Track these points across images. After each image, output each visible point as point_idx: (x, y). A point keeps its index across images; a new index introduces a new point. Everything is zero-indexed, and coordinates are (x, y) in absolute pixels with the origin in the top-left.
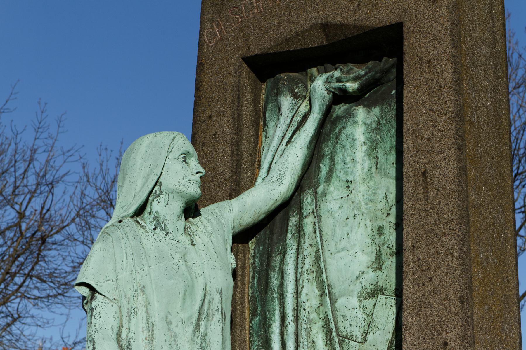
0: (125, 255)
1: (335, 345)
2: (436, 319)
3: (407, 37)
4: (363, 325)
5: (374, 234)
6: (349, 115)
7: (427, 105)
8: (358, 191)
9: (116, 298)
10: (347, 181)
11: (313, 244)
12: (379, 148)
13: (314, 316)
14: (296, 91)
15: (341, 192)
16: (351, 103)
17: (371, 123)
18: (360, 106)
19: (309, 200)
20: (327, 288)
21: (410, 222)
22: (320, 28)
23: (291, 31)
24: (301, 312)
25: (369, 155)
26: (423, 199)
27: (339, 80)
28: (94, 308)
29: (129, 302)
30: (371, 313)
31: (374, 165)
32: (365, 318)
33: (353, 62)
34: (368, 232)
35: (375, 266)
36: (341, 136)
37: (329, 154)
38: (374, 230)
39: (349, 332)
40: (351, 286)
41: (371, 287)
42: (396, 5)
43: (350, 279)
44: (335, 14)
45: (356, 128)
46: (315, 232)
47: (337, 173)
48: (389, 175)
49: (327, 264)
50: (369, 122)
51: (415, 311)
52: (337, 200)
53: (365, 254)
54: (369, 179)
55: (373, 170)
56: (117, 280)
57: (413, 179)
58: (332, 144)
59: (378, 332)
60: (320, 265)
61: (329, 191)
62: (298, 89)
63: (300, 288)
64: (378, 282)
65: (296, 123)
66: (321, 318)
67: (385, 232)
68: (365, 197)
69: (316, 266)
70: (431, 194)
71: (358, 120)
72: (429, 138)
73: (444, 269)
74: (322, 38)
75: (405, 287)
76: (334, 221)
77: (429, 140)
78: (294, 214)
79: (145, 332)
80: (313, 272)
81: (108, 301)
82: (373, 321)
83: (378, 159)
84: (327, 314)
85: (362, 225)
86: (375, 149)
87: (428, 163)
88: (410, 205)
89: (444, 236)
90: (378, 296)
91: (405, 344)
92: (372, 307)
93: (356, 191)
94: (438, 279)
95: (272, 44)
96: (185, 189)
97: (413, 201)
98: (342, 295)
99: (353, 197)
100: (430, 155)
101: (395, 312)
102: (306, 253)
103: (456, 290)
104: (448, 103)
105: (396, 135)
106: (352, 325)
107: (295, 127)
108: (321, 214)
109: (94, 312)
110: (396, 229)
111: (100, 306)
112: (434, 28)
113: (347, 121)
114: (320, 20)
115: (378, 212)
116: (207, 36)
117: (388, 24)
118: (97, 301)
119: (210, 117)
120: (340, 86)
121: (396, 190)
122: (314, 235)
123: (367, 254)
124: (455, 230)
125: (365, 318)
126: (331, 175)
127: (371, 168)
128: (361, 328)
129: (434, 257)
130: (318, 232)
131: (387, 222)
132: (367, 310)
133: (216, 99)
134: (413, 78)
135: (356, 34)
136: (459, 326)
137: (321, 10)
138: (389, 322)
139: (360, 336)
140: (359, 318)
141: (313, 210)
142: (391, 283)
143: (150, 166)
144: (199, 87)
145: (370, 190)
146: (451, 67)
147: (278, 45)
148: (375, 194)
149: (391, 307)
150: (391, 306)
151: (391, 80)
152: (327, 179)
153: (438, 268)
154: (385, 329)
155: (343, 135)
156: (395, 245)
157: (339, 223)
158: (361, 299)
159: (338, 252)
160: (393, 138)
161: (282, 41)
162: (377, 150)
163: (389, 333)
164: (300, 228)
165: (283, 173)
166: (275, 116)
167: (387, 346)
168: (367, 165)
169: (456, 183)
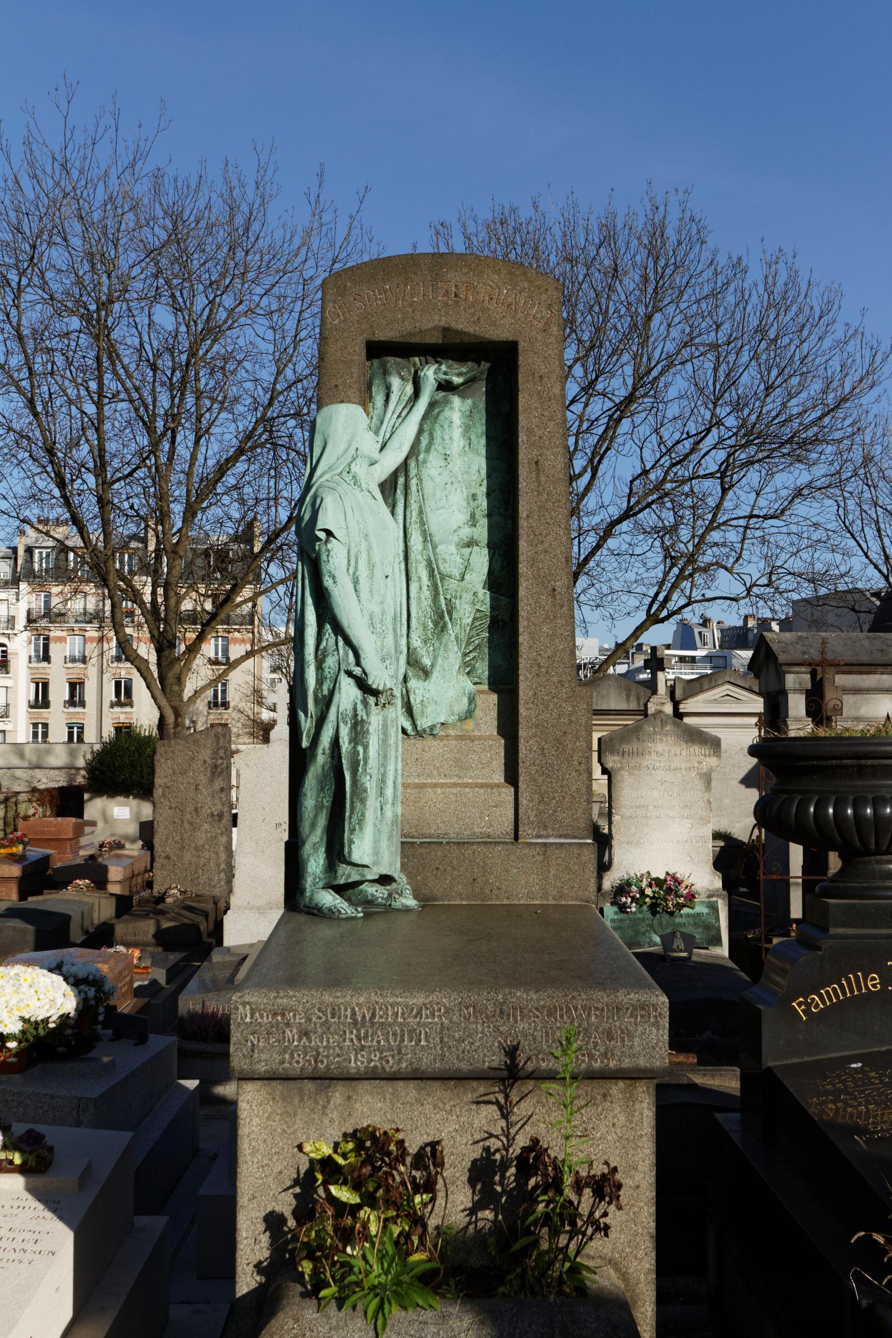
6: (447, 402)
7: (539, 410)
13: (419, 557)
25: (464, 436)
27: (445, 373)
31: (467, 444)
33: (453, 359)
35: (470, 523)
44: (457, 322)
55: (467, 448)
59: (474, 574)
70: (543, 479)
77: (540, 437)
85: (459, 490)
98: (441, 543)
102: (413, 507)
113: (445, 406)
119: (336, 386)
133: (342, 372)
136: (565, 578)
159: (438, 509)
164: (406, 487)
168: (462, 443)
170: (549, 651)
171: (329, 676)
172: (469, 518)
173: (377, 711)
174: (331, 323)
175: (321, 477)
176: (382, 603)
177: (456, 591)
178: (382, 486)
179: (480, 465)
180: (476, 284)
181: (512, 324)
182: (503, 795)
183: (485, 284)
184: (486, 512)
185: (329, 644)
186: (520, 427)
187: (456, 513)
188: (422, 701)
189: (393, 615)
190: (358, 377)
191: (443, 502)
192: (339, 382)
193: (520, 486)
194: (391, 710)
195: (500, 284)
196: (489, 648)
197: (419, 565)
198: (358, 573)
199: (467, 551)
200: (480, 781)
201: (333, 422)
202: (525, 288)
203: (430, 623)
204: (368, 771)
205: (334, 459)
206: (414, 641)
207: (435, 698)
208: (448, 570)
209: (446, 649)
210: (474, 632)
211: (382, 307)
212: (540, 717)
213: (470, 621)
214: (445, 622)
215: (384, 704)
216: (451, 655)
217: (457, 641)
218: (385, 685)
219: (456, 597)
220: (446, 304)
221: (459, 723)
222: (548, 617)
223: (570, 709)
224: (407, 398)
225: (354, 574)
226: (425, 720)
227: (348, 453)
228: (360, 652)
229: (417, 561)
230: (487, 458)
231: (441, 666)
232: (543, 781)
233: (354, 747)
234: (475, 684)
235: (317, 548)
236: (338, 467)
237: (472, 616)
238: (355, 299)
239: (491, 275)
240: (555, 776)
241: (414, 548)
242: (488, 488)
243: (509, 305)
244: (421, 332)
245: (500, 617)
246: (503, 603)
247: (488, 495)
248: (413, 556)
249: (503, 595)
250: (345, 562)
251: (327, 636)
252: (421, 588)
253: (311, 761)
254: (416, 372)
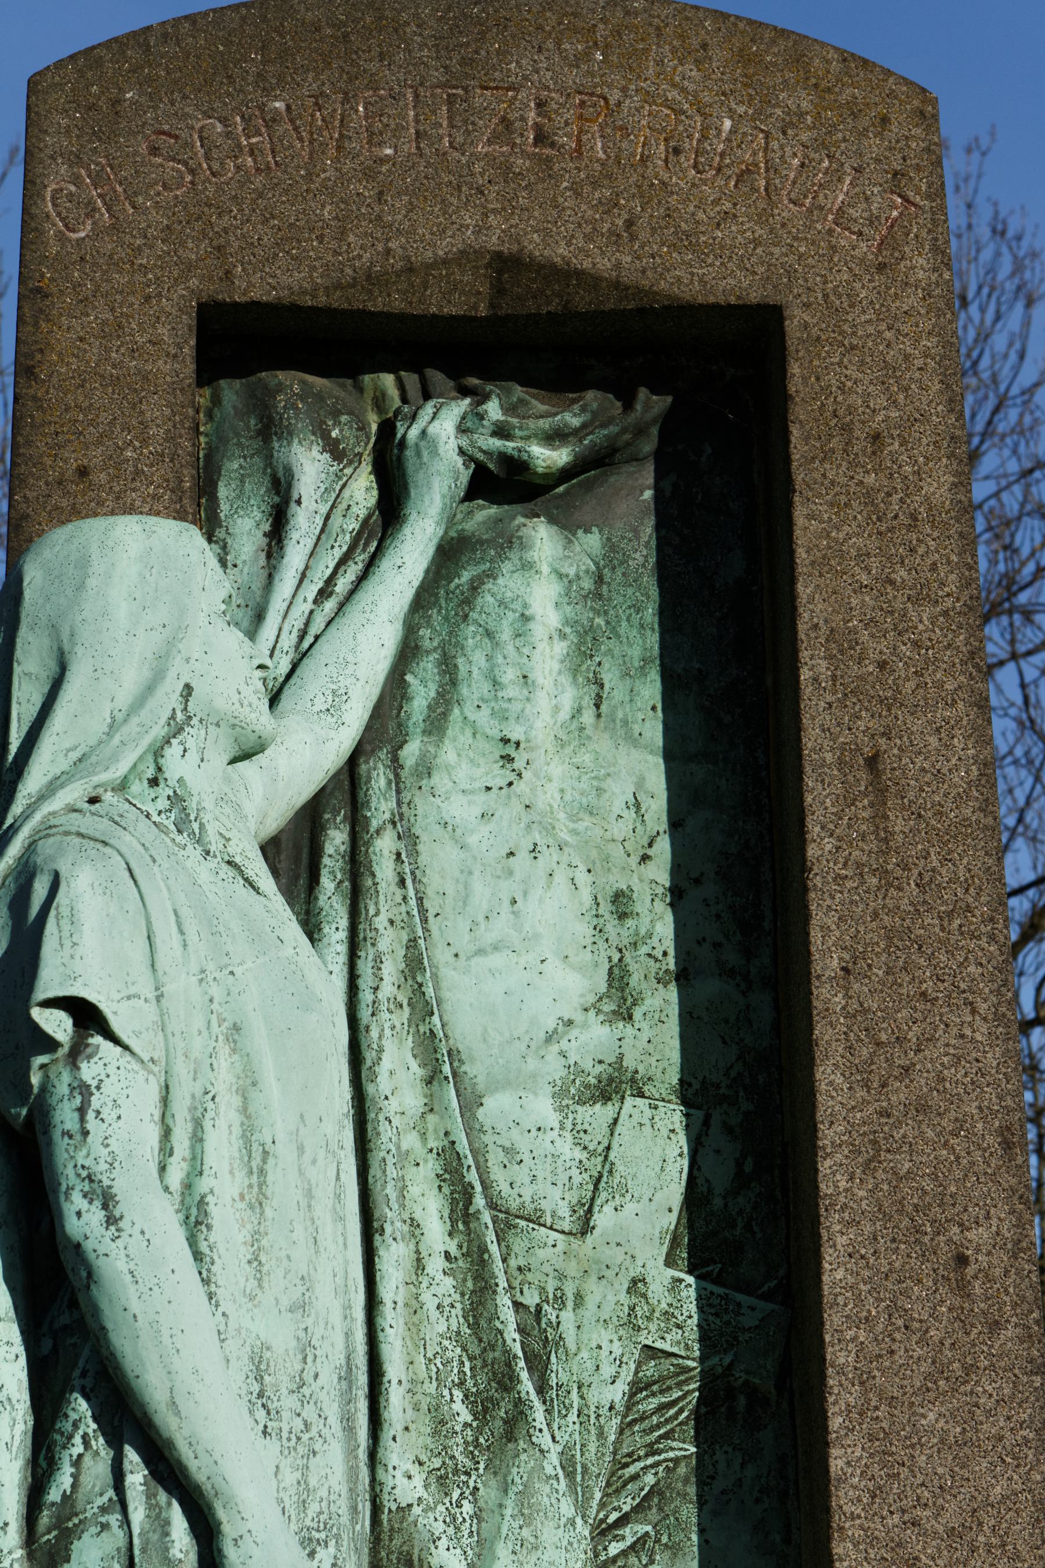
0: (173, 918)
1: (484, 1235)
2: (928, 1185)
3: (797, 351)
4: (577, 1179)
5: (601, 912)
7: (874, 563)
8: (542, 775)
9: (156, 1058)
10: (502, 740)
11: (397, 919)
12: (605, 654)
13: (411, 1141)
14: (334, 434)
16: (509, 503)
18: (538, 516)
19: (382, 782)
20: (446, 1059)
22: (488, 266)
23: (388, 251)
24: (381, 1129)
25: (575, 672)
26: (872, 837)
27: (501, 431)
28: (94, 1083)
29: (195, 1073)
30: (600, 1149)
31: (588, 702)
32: (581, 1162)
34: (581, 904)
35: (608, 1007)
36: (480, 600)
37: (435, 649)
39: (527, 1198)
40: (529, 1060)
41: (599, 1068)
42: (759, 251)
44: (546, 233)
45: (533, 584)
46: (402, 883)
47: (466, 710)
48: (642, 741)
49: (444, 984)
50: (572, 572)
53: (572, 967)
54: (576, 743)
55: (588, 717)
56: (159, 998)
57: (836, 772)
58: (446, 619)
59: (630, 1208)
60: (421, 985)
61: (438, 760)
62: (341, 431)
63: (374, 1053)
64: (621, 1057)
66: (431, 1150)
67: (638, 908)
68: (568, 797)
70: (899, 824)
71: (536, 558)
72: (885, 663)
73: (947, 1045)
74: (479, 293)
75: (823, 1086)
77: (882, 665)
78: (338, 819)
79: (237, 1173)
80: (401, 1006)
81: (135, 1065)
82: (610, 1172)
83: (602, 686)
84: (452, 1138)
85: (561, 877)
86: (592, 656)
87: (883, 734)
88: (828, 847)
89: (943, 951)
90: (623, 1098)
91: (831, 1251)
93: (536, 775)
94: (928, 1072)
95: (319, 281)
96: (253, 716)
97: (840, 839)
98: (497, 1086)
99: (528, 790)
100: (889, 710)
101: (685, 1150)
102: (383, 945)
103: (988, 1108)
104: (942, 570)
105: (661, 624)
106: (540, 1178)
107: (345, 548)
108: (417, 830)
109: (93, 1098)
111: (113, 1078)
112: (885, 343)
113: (501, 556)
114: (494, 239)
115: (611, 846)
116: (54, 205)
117: (733, 300)
118: (101, 1063)
119: (83, 472)
120: (510, 451)
121: (669, 789)
122: (399, 893)
123: (580, 969)
124: (979, 938)
125: (581, 1162)
126: (444, 714)
130: (409, 882)
131: (641, 881)
132: (586, 1138)
133: (105, 417)
134: (824, 475)
135: (609, 306)
136: (1001, 1211)
137: (494, 211)
138: (669, 1178)
139: (567, 1214)
140: (563, 1158)
141: (393, 814)
142: (666, 1064)
143: (160, 629)
144: (33, 367)
145: (584, 778)
146: (946, 466)
147: (338, 286)
149: (672, 1135)
150: (673, 1131)
151: (641, 456)
152: (432, 723)
153: (928, 1040)
154: (656, 1198)
156: (672, 952)
157: (483, 865)
158: (564, 1103)
159: (481, 952)
160: (649, 632)
161: (354, 279)
162: (598, 659)
163: (670, 1210)
165: (342, 691)
166: (252, 502)
167: (665, 1249)
168: (568, 699)
169: (977, 805)
170: (952, 1507)
172: (603, 987)
174: (61, 237)
175: (43, 797)
176: (301, 1307)
177: (561, 1276)
179: (640, 783)
180: (615, 96)
181: (756, 242)
183: (649, 98)
184: (671, 963)
185: (86, 1480)
186: (802, 628)
187: (553, 965)
190: (170, 438)
191: (501, 926)
192: (96, 456)
193: (812, 851)
195: (706, 97)
196: (701, 1503)
197: (411, 1172)
198: (204, 1185)
201: (92, 582)
202: (801, 115)
203: (458, 1406)
205: (98, 727)
206: (401, 1481)
208: (527, 1194)
209: (527, 1514)
210: (637, 1440)
211: (259, 181)
213: (617, 1393)
214: (519, 1402)
216: (550, 1534)
217: (570, 1475)
219: (560, 1300)
220: (506, 168)
222: (941, 1370)
224: (353, 525)
225: (188, 1186)
227: (151, 704)
228: (221, 1514)
229: (404, 1155)
230: (669, 755)
235: (35, 1079)
236: (115, 758)
237: (627, 1374)
238: (154, 151)
239: (670, 64)
241: (392, 1107)
242: (676, 869)
243: (745, 175)
244: (410, 270)
245: (739, 1376)
246: (749, 1320)
247: (677, 895)
249: (748, 1289)
250: (152, 1134)
251: (78, 1449)
252: (419, 1265)
254: (387, 429)
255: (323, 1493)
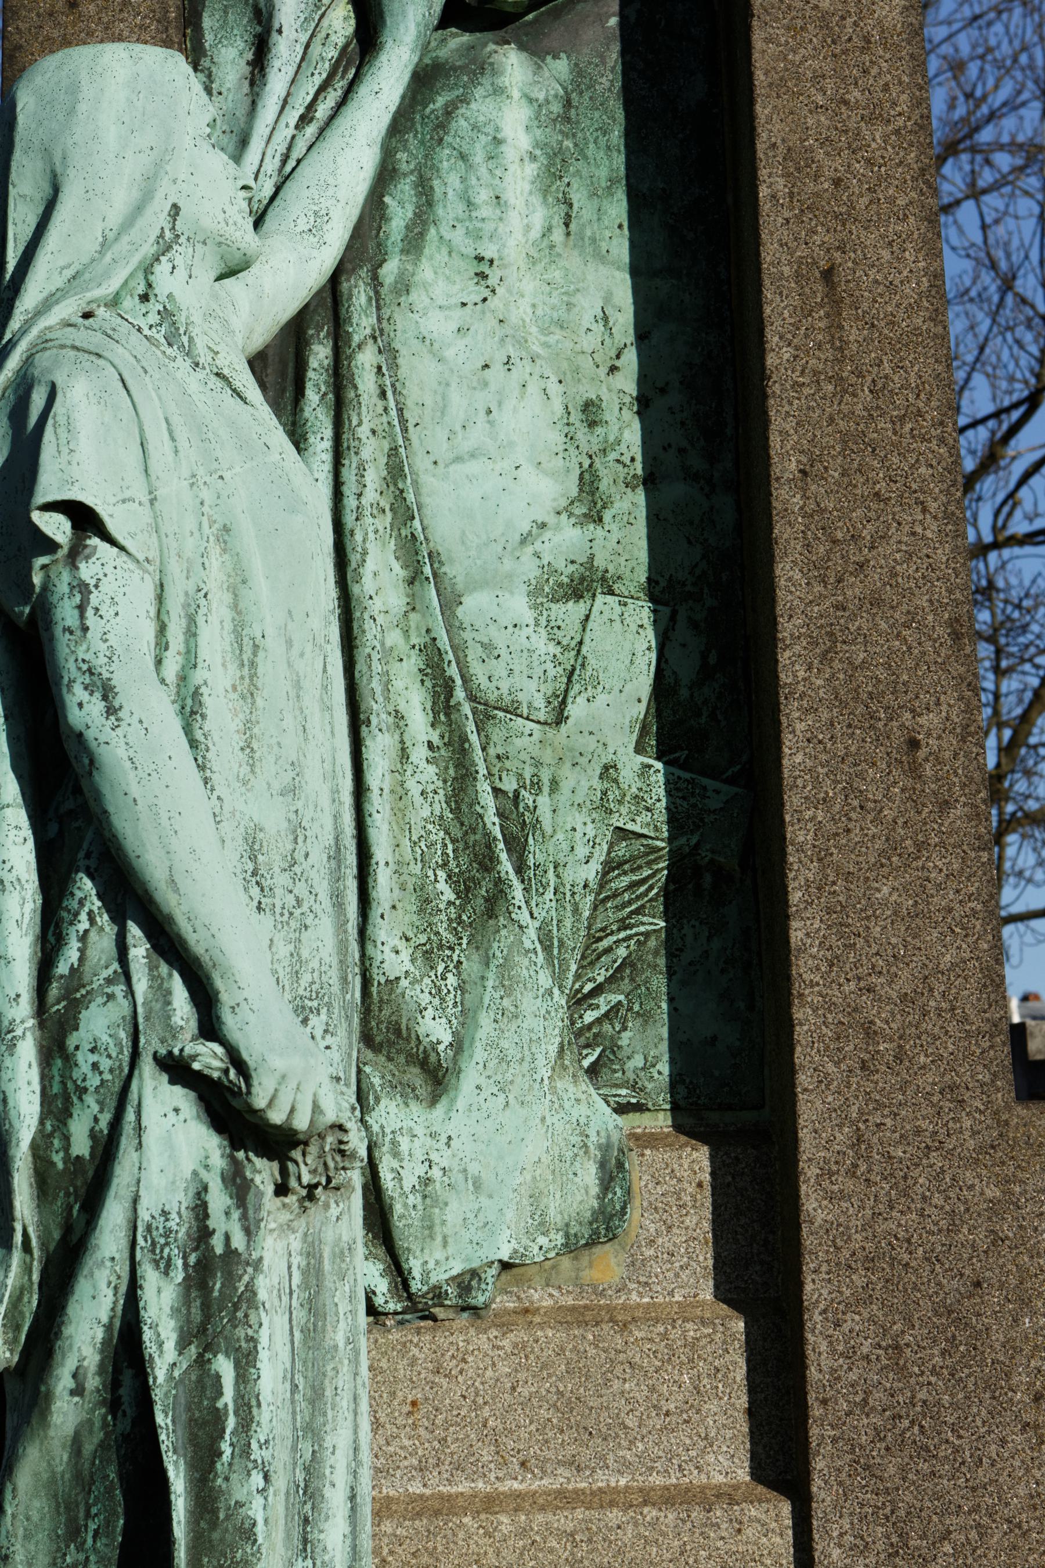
0: (164, 425)
1: (465, 726)
5: (571, 420)
7: (829, 85)
10: (476, 258)
11: (379, 429)
12: (574, 175)
13: (394, 638)
15: (457, 287)
16: (481, 31)
17: (547, 101)
21: (791, 404)
24: (366, 627)
25: (545, 192)
26: (828, 346)
28: (92, 582)
30: (573, 643)
31: (558, 221)
34: (553, 413)
35: (580, 510)
36: (454, 124)
37: (412, 172)
38: (571, 409)
39: (505, 691)
40: (505, 561)
41: (572, 568)
43: (503, 541)
45: (504, 108)
46: (383, 394)
47: (442, 230)
48: (610, 258)
49: (424, 491)
50: (541, 96)
51: (818, 651)
52: (449, 308)
53: (545, 473)
54: (547, 260)
55: (558, 235)
57: (793, 285)
58: (422, 142)
59: (602, 699)
60: (402, 491)
61: (416, 278)
63: (358, 556)
64: (592, 557)
65: (327, 65)
66: (414, 647)
67: (607, 416)
68: (539, 312)
69: (392, 496)
70: (853, 334)
71: (507, 84)
73: (900, 542)
76: (440, 368)
77: (837, 182)
79: (229, 666)
80: (384, 511)
81: (131, 565)
82: (583, 665)
83: (571, 205)
84: (433, 635)
85: (533, 388)
86: (561, 177)
87: (838, 248)
88: (786, 356)
89: (895, 454)
90: (594, 595)
91: (790, 736)
92: (578, 626)
93: (509, 291)
96: (238, 234)
98: (475, 586)
100: (844, 225)
101: (653, 644)
102: (366, 453)
104: (894, 91)
105: (626, 146)
106: (516, 672)
107: (324, 75)
108: (396, 345)
109: (92, 596)
110: (638, 413)
111: (111, 577)
113: (474, 82)
115: (581, 357)
118: (98, 563)
121: (635, 303)
122: (381, 404)
123: (552, 474)
127: (550, 229)
128: (546, 681)
129: (869, 509)
130: (389, 394)
131: (610, 390)
136: (950, 698)
138: (638, 671)
139: (542, 706)
140: (537, 652)
141: (373, 330)
143: (148, 151)
145: (555, 294)
148: (569, 305)
150: (641, 626)
153: (881, 537)
154: (625, 690)
155: (462, 122)
156: (639, 458)
157: (460, 377)
158: (539, 601)
159: (458, 459)
160: (615, 154)
163: (639, 701)
165: (323, 212)
166: (235, 32)
167: (635, 737)
168: (539, 218)
169: (928, 314)
170: (904, 974)
171: (94, 1081)
172: (574, 492)
173: (285, 1217)
176: (292, 791)
177: (538, 764)
178: (257, 363)
179: (608, 298)
182: (749, 1532)
184: (638, 468)
185: (93, 954)
186: (761, 147)
187: (527, 472)
188: (426, 1181)
189: (328, 839)
191: (478, 435)
193: (771, 360)
194: (334, 1211)
196: (670, 973)
197: (395, 667)
198: (198, 676)
199: (572, 611)
200: (657, 1480)
204: (256, 1454)
205: (90, 246)
206: (389, 955)
207: (473, 1169)
209: (507, 985)
210: (610, 916)
212: (881, 1227)
213: (591, 872)
214: (499, 881)
215: (312, 1188)
216: (529, 1004)
217: (547, 949)
218: (316, 1108)
219: (536, 786)
221: (566, 1262)
222: (894, 846)
223: (993, 1192)
224: (332, 53)
225: (183, 678)
226: (439, 1255)
227: (141, 223)
228: (219, 983)
229: (388, 652)
230: (635, 271)
231: (490, 1045)
232: (903, 1469)
233: (201, 1363)
234: (622, 1109)
235: (37, 579)
236: (107, 275)
237: (600, 854)
240: (945, 1451)
241: (376, 606)
242: (643, 378)
245: (705, 855)
247: (644, 404)
248: (370, 635)
251: (84, 925)
252: (404, 754)
253: (25, 1420)
255: (314, 964)
